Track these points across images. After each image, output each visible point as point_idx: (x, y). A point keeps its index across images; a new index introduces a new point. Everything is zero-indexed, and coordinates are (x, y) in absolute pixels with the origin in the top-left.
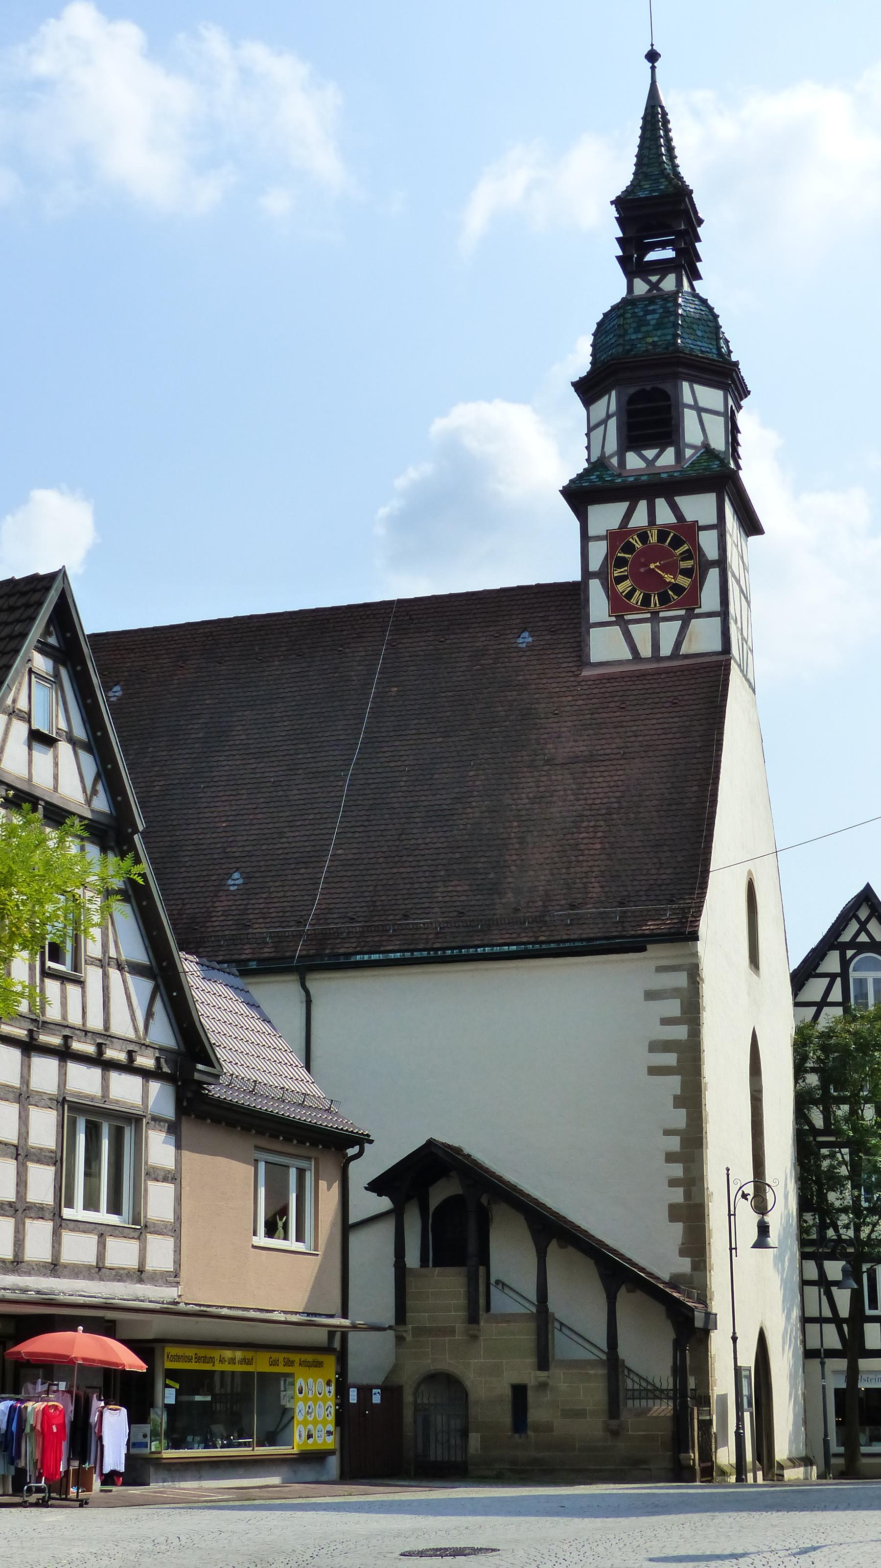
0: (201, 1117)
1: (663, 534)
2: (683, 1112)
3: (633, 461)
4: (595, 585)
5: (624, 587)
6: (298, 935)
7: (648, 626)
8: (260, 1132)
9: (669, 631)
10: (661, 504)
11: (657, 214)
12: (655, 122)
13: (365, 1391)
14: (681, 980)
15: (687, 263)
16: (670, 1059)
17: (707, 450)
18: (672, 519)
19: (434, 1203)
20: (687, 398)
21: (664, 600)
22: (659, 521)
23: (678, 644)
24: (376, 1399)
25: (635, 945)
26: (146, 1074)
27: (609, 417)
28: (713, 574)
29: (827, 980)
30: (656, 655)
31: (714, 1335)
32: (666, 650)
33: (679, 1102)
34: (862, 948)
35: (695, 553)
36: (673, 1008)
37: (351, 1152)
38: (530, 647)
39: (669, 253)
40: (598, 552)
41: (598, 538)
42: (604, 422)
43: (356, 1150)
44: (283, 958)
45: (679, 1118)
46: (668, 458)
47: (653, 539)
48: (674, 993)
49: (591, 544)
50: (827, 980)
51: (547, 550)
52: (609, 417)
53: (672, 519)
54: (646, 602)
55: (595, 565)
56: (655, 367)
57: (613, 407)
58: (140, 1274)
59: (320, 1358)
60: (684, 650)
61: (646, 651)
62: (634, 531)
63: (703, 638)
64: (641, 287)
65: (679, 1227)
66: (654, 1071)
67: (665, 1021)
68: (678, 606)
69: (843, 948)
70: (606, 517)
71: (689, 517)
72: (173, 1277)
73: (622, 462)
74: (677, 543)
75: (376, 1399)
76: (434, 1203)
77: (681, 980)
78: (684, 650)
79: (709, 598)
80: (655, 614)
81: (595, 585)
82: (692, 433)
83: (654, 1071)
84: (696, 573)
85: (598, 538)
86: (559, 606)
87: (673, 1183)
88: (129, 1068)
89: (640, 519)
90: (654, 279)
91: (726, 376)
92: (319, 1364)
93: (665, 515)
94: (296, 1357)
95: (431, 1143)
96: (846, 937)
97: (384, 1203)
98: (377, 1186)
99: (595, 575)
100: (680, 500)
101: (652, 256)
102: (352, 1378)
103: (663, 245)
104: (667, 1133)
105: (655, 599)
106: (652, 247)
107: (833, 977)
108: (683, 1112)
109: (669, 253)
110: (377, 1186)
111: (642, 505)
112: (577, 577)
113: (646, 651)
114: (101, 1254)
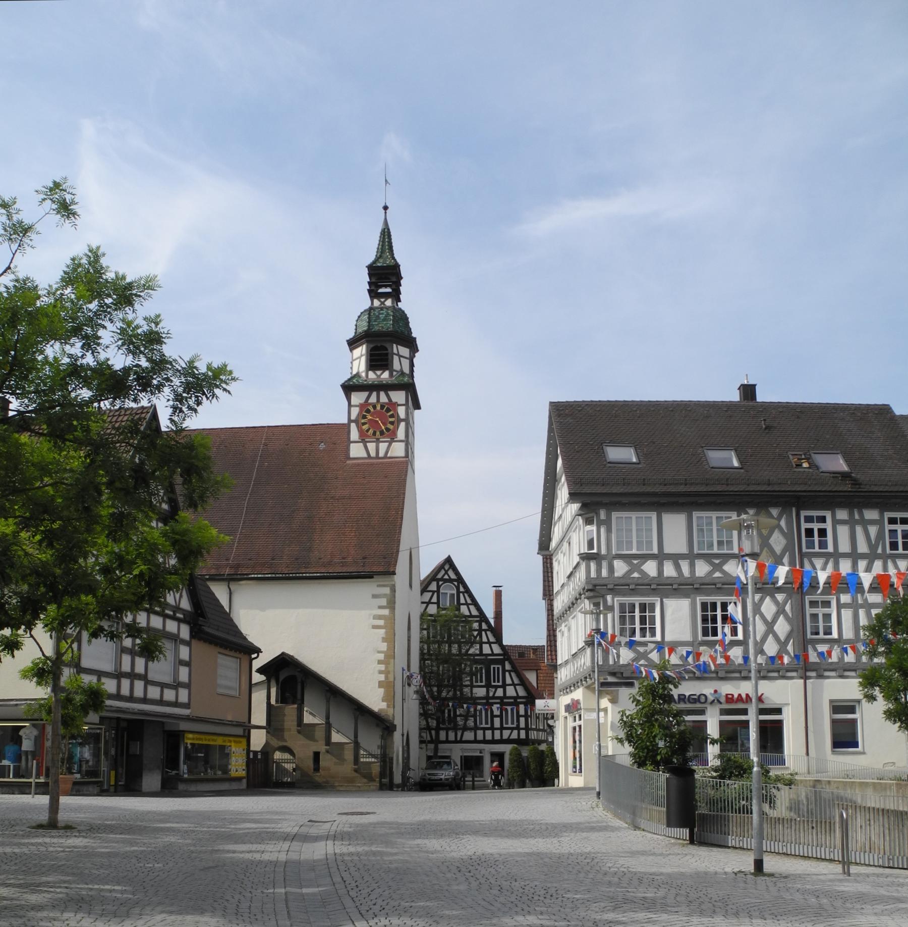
0: (200, 639)
1: (382, 407)
2: (386, 644)
3: (372, 375)
4: (353, 426)
5: (365, 427)
6: (227, 565)
7: (374, 444)
8: (221, 646)
9: (383, 447)
10: (382, 394)
11: (385, 276)
12: (386, 235)
13: (255, 753)
14: (387, 591)
15: (396, 295)
16: (381, 622)
17: (402, 373)
18: (386, 400)
19: (282, 678)
20: (395, 351)
21: (382, 433)
22: (381, 401)
23: (387, 452)
24: (259, 757)
25: (369, 576)
26: (179, 621)
27: (362, 355)
28: (403, 425)
29: (431, 594)
30: (377, 457)
31: (395, 733)
32: (381, 454)
33: (384, 640)
34: (445, 581)
35: (395, 415)
36: (383, 602)
37: (253, 656)
38: (324, 450)
39: (389, 290)
40: (355, 412)
41: (356, 406)
42: (360, 358)
43: (255, 655)
44: (220, 575)
45: (384, 646)
46: (386, 375)
47: (378, 408)
48: (384, 596)
49: (352, 409)
50: (431, 594)
51: (334, 409)
52: (362, 355)
53: (386, 400)
54: (374, 434)
55: (353, 417)
56: (386, 338)
57: (364, 352)
58: (176, 704)
59: (241, 739)
60: (389, 455)
61: (373, 454)
62: (370, 404)
63: (398, 450)
64: (377, 303)
65: (382, 690)
66: (375, 627)
67: (380, 607)
68: (388, 436)
69: (438, 580)
70: (358, 398)
71: (394, 400)
72: (187, 706)
73: (367, 375)
74: (388, 410)
75: (259, 757)
76: (282, 678)
77: (387, 591)
78: (389, 455)
79: (401, 433)
80: (378, 439)
81: (353, 426)
82: (396, 366)
83: (375, 627)
84: (396, 424)
85: (356, 406)
86: (334, 434)
87: (380, 672)
88: (173, 618)
89: (373, 399)
90: (382, 300)
91: (411, 344)
92: (240, 742)
93: (383, 398)
94: (231, 739)
95: (283, 653)
96: (439, 576)
97: (262, 678)
98: (261, 671)
99: (353, 421)
100: (390, 393)
101: (380, 290)
102: (252, 748)
103: (386, 286)
104: (379, 652)
105: (378, 433)
106: (381, 287)
107: (433, 592)
108: (386, 644)
109: (389, 290)
110: (261, 671)
111: (374, 394)
112: (345, 421)
113: (373, 454)
114: (162, 692)
